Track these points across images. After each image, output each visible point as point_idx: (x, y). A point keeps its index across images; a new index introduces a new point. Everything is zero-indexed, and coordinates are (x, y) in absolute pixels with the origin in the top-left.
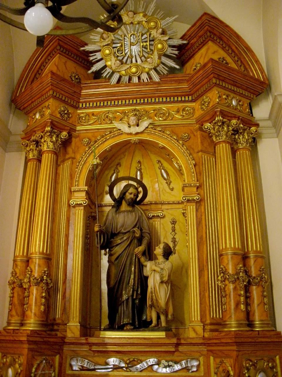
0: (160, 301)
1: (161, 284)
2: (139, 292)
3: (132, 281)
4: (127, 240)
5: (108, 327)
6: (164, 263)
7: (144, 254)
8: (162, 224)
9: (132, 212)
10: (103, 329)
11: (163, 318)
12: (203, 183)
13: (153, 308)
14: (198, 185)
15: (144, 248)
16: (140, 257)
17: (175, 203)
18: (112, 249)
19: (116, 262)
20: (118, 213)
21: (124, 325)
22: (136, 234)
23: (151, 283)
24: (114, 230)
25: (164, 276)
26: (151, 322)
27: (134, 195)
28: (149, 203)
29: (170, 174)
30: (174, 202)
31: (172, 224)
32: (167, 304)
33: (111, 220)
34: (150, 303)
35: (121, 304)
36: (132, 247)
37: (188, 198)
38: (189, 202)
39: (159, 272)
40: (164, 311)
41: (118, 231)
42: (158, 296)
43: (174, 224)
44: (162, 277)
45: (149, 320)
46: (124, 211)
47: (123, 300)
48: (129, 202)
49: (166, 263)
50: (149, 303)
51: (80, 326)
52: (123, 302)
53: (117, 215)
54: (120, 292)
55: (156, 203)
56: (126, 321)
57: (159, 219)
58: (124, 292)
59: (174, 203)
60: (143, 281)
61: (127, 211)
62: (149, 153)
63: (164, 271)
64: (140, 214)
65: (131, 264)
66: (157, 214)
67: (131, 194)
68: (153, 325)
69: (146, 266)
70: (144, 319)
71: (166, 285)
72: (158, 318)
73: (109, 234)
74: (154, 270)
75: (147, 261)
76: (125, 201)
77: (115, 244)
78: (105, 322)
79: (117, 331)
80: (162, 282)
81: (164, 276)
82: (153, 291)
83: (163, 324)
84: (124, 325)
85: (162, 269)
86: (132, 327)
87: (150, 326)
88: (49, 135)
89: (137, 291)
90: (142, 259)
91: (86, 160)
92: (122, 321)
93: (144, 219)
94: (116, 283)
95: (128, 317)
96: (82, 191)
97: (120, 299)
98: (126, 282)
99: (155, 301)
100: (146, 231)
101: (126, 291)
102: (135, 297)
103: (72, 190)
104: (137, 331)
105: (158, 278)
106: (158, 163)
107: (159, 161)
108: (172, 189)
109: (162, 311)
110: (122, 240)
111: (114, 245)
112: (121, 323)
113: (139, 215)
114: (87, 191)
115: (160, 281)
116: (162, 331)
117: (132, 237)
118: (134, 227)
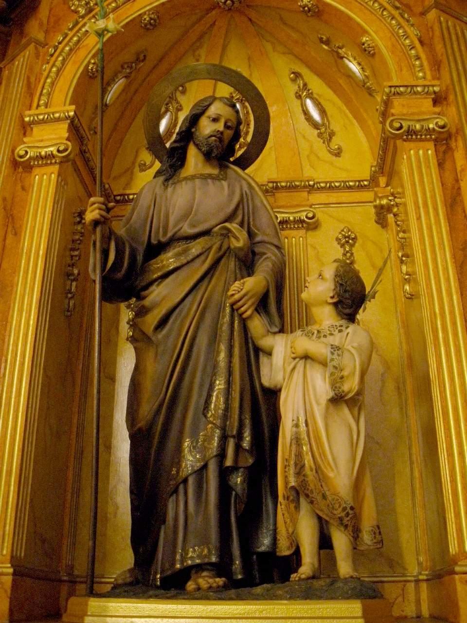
0: (331, 475)
1: (331, 408)
2: (246, 444)
3: (217, 401)
4: (203, 258)
5: (128, 580)
6: (340, 331)
7: (262, 305)
8: (312, 246)
9: (220, 180)
10: (108, 588)
11: (340, 540)
12: (451, 87)
13: (303, 501)
14: (436, 89)
15: (264, 283)
16: (249, 313)
17: (350, 187)
18: (147, 292)
19: (161, 335)
20: (174, 183)
21: (186, 574)
22: (232, 239)
23: (290, 409)
24: (158, 232)
25: (345, 373)
26: (296, 557)
27: (226, 127)
28: (271, 185)
29: (329, 113)
30: (345, 182)
31: (342, 246)
32: (357, 485)
33: (149, 207)
34: (293, 482)
35: (176, 491)
36: (217, 281)
37: (410, 123)
38: (411, 140)
39: (324, 364)
40: (347, 515)
41: (169, 234)
42: (323, 454)
43: (352, 246)
44: (336, 381)
45: (284, 550)
46: (193, 178)
47: (183, 474)
48: (208, 145)
49: (350, 330)
50: (286, 483)
51: (15, 574)
52: (185, 481)
53: (170, 190)
54: (171, 445)
55: (292, 188)
56: (193, 556)
57: (302, 232)
58: (187, 443)
59: (347, 188)
60: (262, 406)
61: (201, 175)
62: (269, 47)
63: (346, 355)
64: (245, 188)
65: (214, 339)
66: (297, 216)
67: (215, 120)
68: (306, 569)
69: (269, 354)
70: (263, 549)
71: (352, 413)
72: (325, 543)
73: (141, 250)
74: (306, 357)
75: (275, 333)
76: (197, 145)
77: (159, 274)
78: (122, 559)
79: (157, 597)
80: (337, 400)
81: (345, 373)
82: (304, 436)
83: (345, 568)
84: (186, 574)
85: (335, 348)
86: (220, 581)
87: (294, 576)
88: (171, 480)
89: (239, 437)
90: (257, 325)
91: (79, 41)
92: (178, 557)
93: (259, 204)
94: (158, 412)
95: (204, 541)
96: (58, 120)
97: (174, 472)
98: (196, 409)
99: (310, 475)
100: (266, 239)
101: (194, 435)
102: (229, 462)
103: (27, 119)
104: (239, 598)
105: (321, 386)
106: (293, 81)
107: (297, 75)
108: (338, 153)
109: (339, 513)
110: (183, 260)
111: (155, 276)
112: (173, 564)
113: (241, 189)
114: (72, 122)
115: (331, 394)
116: (347, 597)
117: (220, 248)
118: (230, 219)
